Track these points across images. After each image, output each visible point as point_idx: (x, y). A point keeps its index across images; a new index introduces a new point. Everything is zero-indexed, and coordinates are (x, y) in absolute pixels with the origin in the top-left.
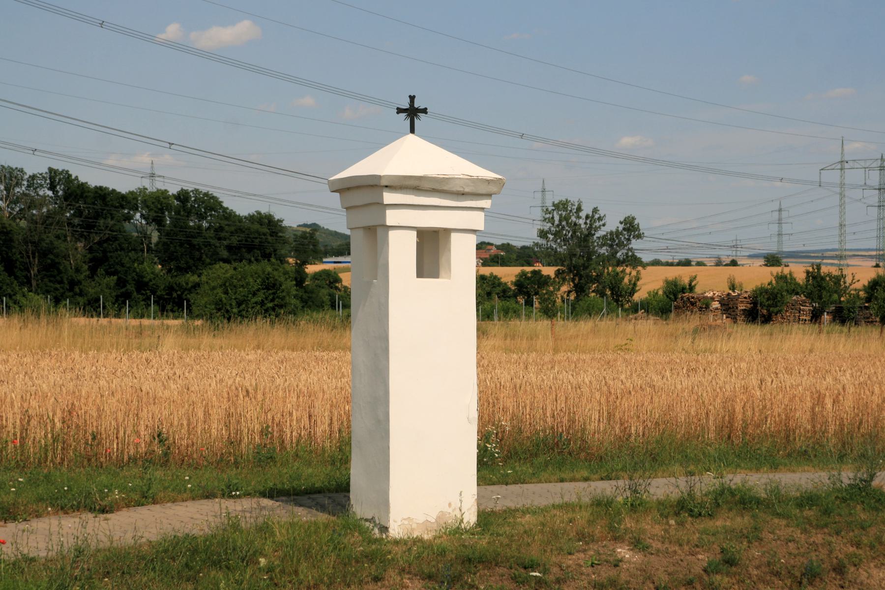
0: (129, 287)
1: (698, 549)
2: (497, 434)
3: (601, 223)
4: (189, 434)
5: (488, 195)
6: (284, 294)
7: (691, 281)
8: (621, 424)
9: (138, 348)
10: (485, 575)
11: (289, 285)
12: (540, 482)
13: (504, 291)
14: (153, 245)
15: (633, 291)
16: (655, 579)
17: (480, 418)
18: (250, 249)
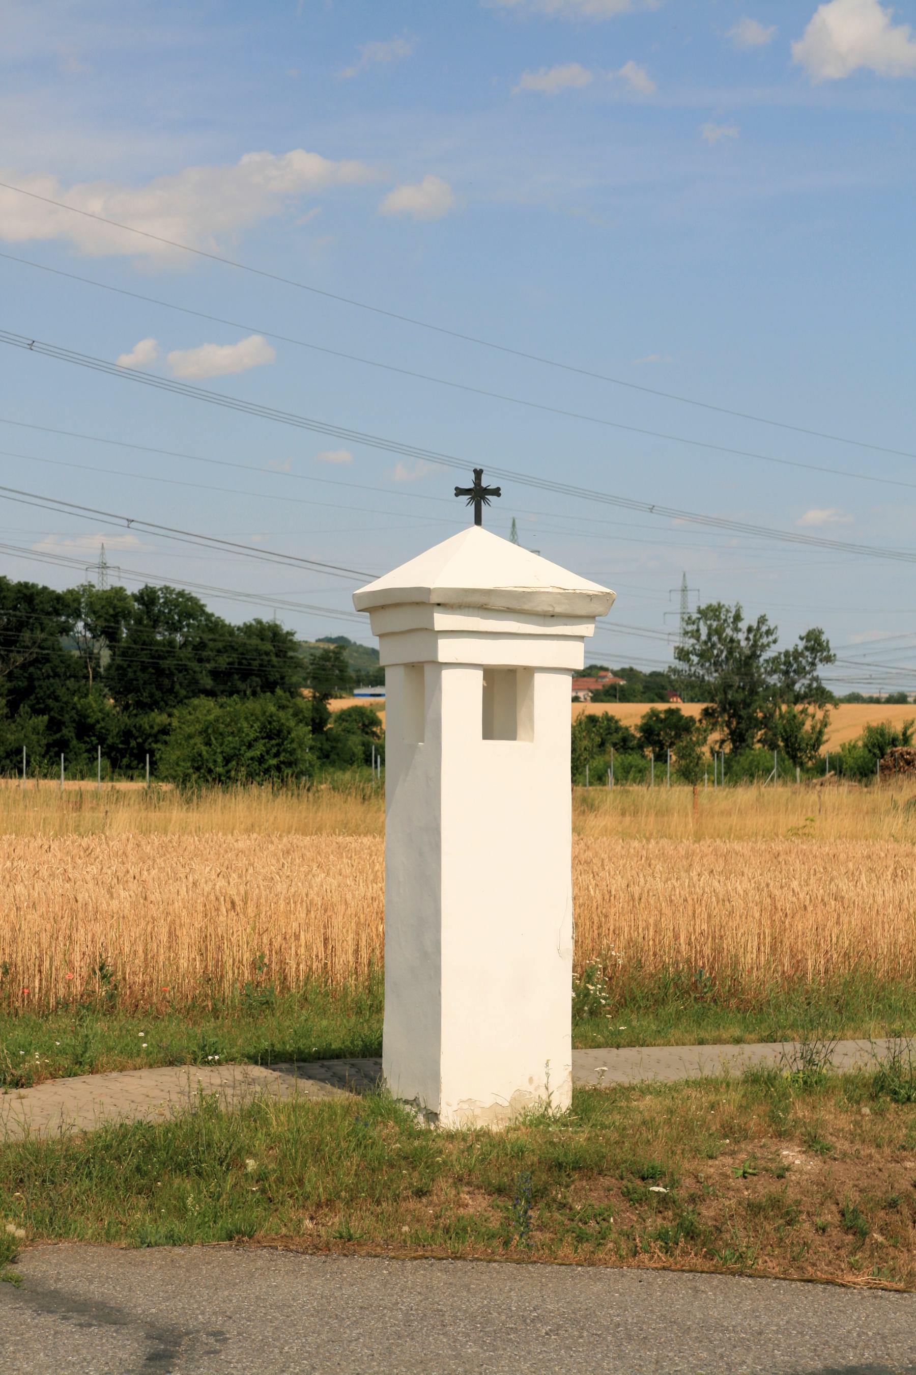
0: (65, 731)
1: (905, 1153)
2: (605, 969)
3: (771, 638)
4: (146, 967)
5: (591, 618)
6: (294, 745)
7: (906, 729)
8: (793, 957)
9: (77, 828)
10: (583, 1188)
11: (303, 732)
12: (668, 1044)
13: (625, 740)
14: (102, 670)
15: (817, 743)
16: (840, 1198)
17: (578, 944)
18: (245, 675)
